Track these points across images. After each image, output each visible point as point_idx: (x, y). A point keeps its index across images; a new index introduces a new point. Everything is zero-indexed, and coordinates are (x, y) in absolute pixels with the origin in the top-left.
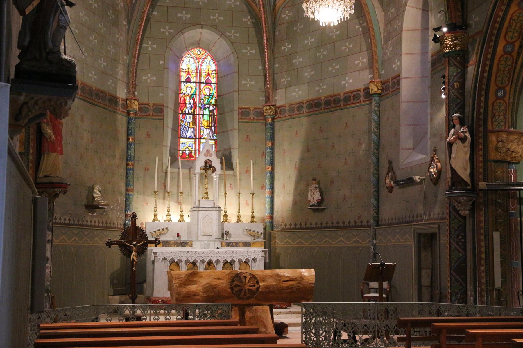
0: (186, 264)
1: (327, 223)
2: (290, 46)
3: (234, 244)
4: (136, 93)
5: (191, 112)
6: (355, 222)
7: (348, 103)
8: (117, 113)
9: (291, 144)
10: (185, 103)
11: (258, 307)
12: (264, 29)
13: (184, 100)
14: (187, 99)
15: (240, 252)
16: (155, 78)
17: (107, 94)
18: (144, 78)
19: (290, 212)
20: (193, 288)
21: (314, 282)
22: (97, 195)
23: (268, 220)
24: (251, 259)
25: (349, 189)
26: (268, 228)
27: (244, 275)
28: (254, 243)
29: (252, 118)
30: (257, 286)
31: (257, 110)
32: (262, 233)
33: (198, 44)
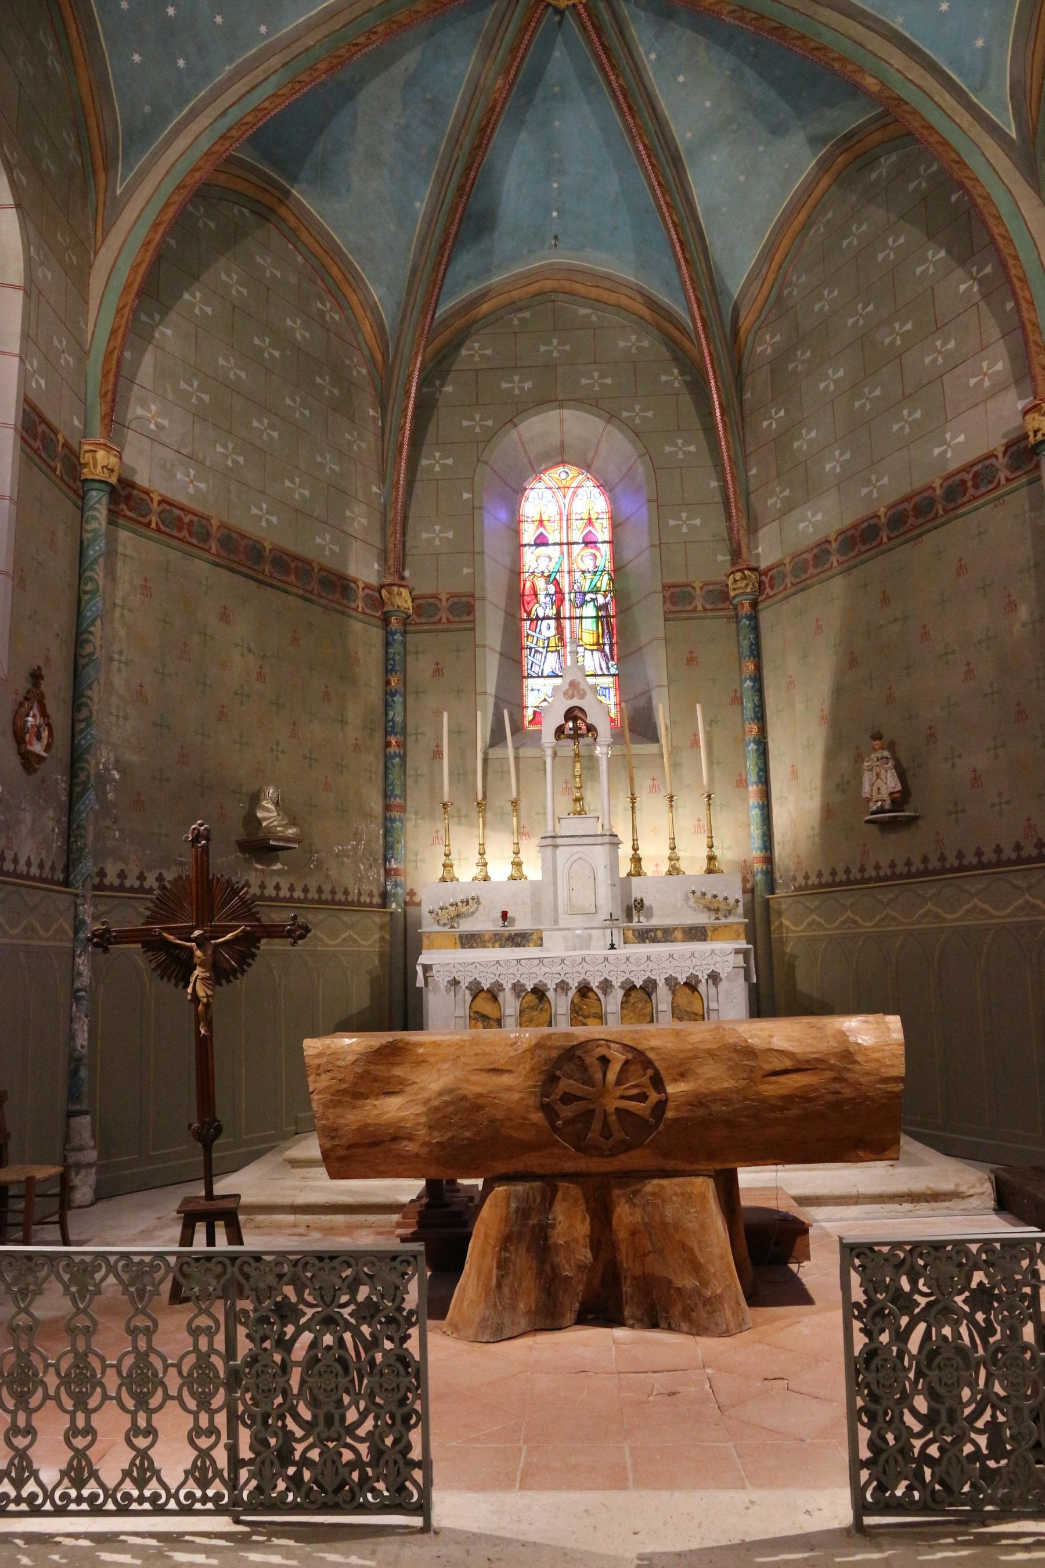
0: (518, 996)
1: (925, 860)
2: (782, 413)
3: (659, 933)
4: (407, 574)
5: (551, 612)
6: (1018, 847)
7: (960, 501)
8: (350, 616)
9: (805, 656)
10: (536, 595)
11: (665, 1182)
12: (712, 381)
13: (534, 587)
14: (541, 584)
15: (671, 956)
16: (450, 535)
17: (315, 565)
18: (425, 536)
19: (817, 839)
20: (392, 1109)
21: (900, 1071)
22: (268, 814)
23: (758, 867)
24: (703, 977)
25: (988, 750)
26: (760, 889)
27: (600, 1051)
28: (715, 929)
29: (700, 608)
30: (654, 1097)
31: (710, 587)
32: (737, 901)
33: (560, 456)
